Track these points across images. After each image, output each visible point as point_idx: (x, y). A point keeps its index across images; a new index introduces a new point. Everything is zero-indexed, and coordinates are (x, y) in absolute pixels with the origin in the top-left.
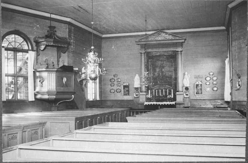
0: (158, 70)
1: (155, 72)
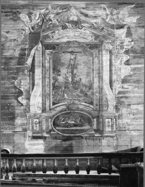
0: (64, 71)
1: (59, 75)
